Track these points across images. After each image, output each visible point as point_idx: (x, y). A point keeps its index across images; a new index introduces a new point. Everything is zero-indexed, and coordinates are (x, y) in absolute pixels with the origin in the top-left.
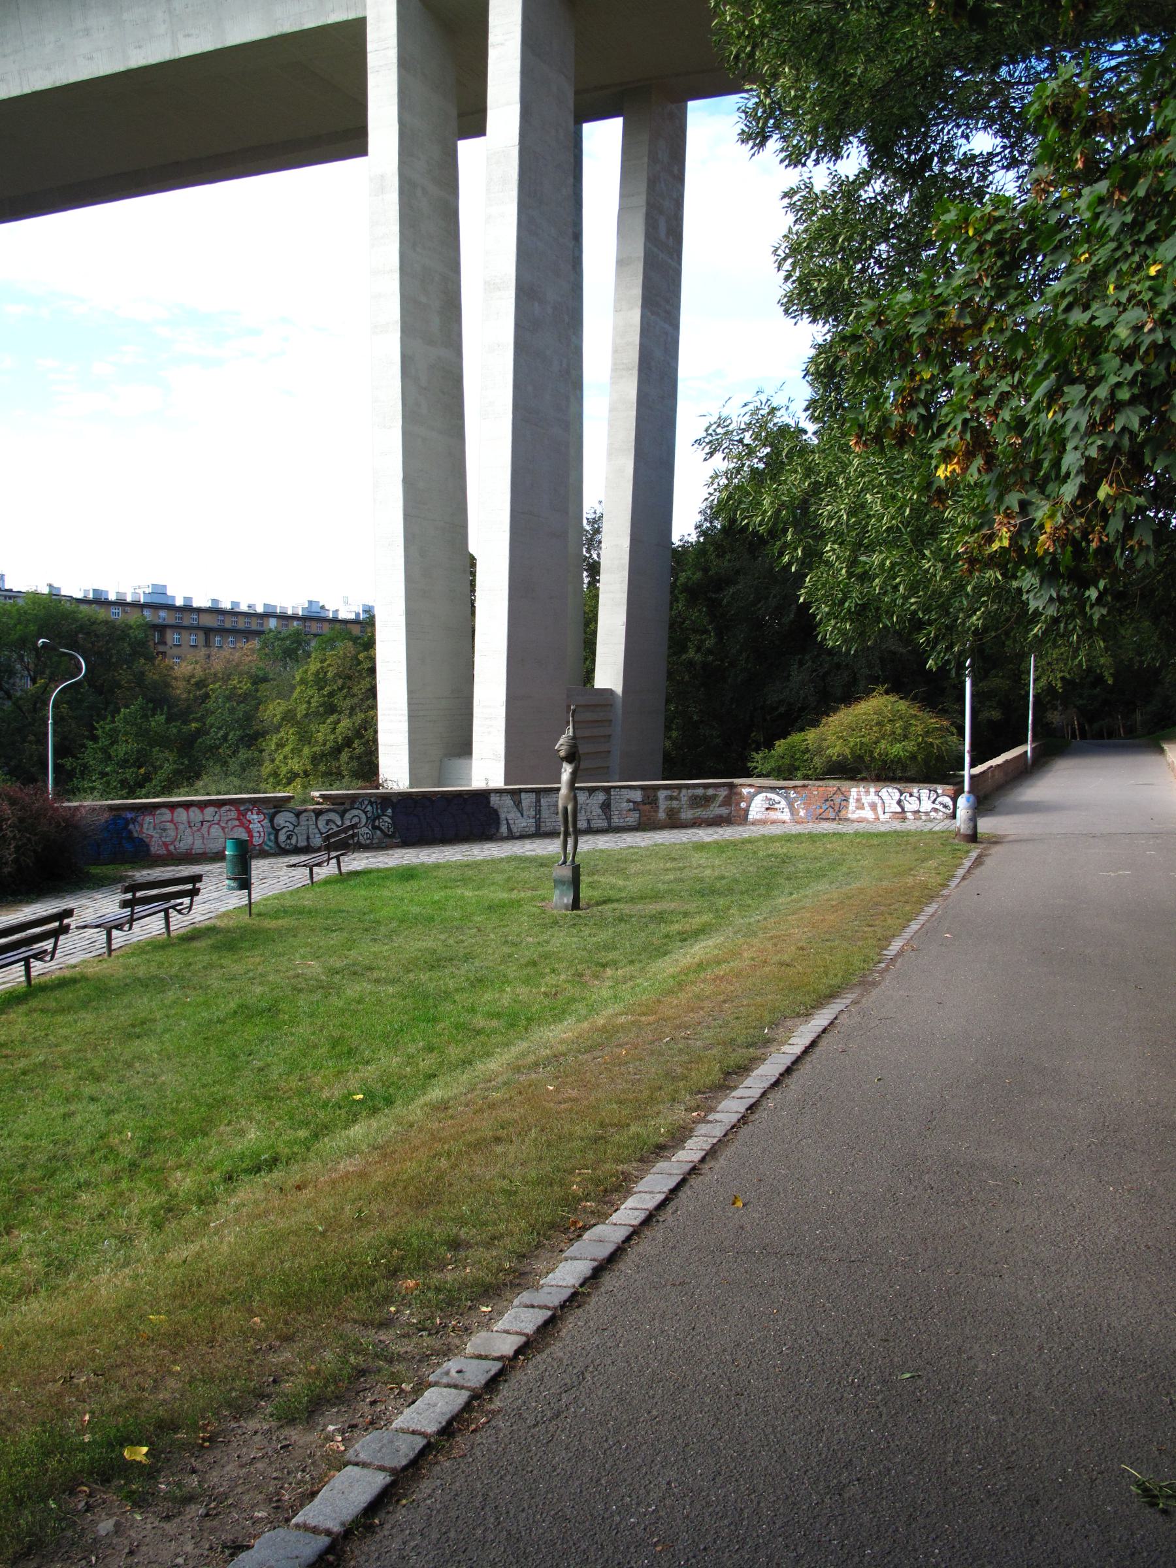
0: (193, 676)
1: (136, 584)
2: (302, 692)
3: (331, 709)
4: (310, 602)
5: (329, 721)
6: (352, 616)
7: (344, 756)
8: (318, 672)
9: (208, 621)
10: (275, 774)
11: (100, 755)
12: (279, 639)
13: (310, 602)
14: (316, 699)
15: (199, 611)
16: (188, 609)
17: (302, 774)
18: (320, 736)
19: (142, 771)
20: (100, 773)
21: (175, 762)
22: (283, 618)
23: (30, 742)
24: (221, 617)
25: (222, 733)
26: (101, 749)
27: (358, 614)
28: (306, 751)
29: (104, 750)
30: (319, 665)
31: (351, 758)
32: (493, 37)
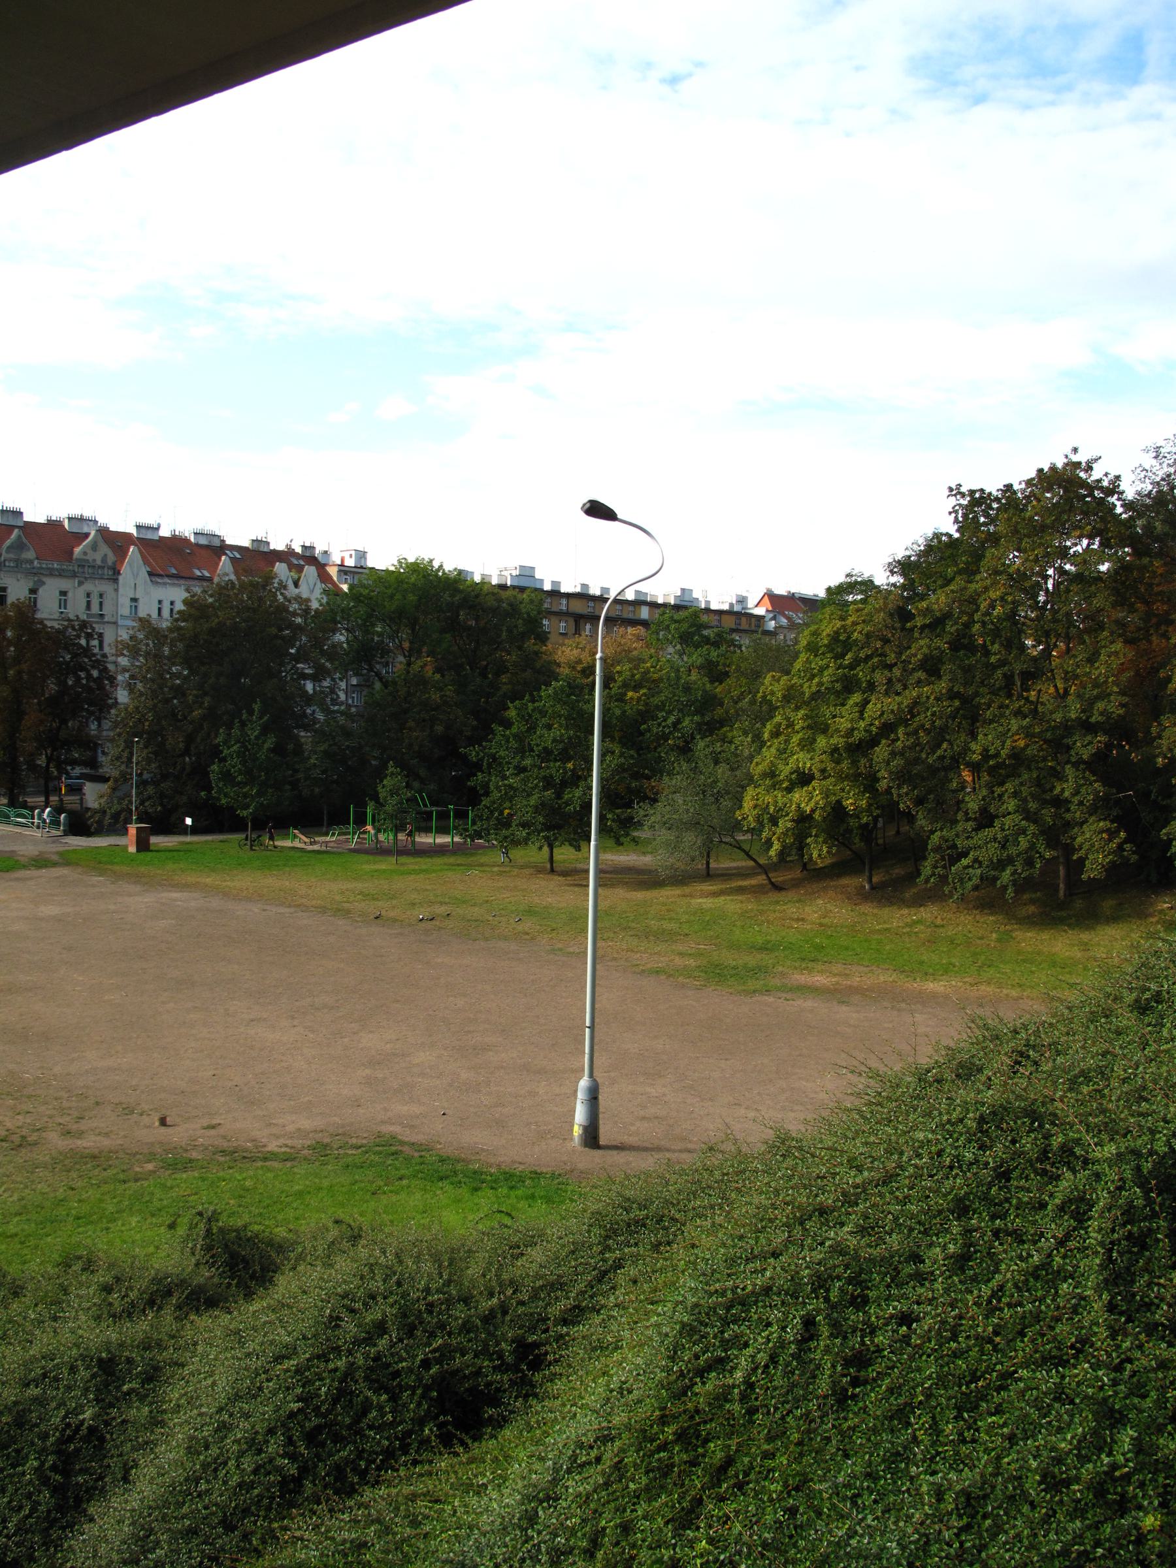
0: (579, 662)
1: (502, 567)
2: (808, 661)
3: (848, 686)
4: (683, 590)
5: (851, 702)
6: (726, 607)
7: (881, 752)
8: (837, 633)
9: (578, 607)
10: (772, 774)
11: (514, 744)
12: (676, 621)
13: (683, 590)
14: (830, 671)
15: (568, 596)
16: (555, 593)
17: (817, 775)
18: (844, 724)
19: (570, 765)
20: (516, 767)
21: (622, 755)
22: (654, 605)
23: (410, 729)
24: (591, 604)
25: (672, 719)
26: (515, 736)
27: (731, 605)
28: (821, 742)
29: (518, 737)
30: (839, 624)
31: (893, 754)
32: (83, 838)
